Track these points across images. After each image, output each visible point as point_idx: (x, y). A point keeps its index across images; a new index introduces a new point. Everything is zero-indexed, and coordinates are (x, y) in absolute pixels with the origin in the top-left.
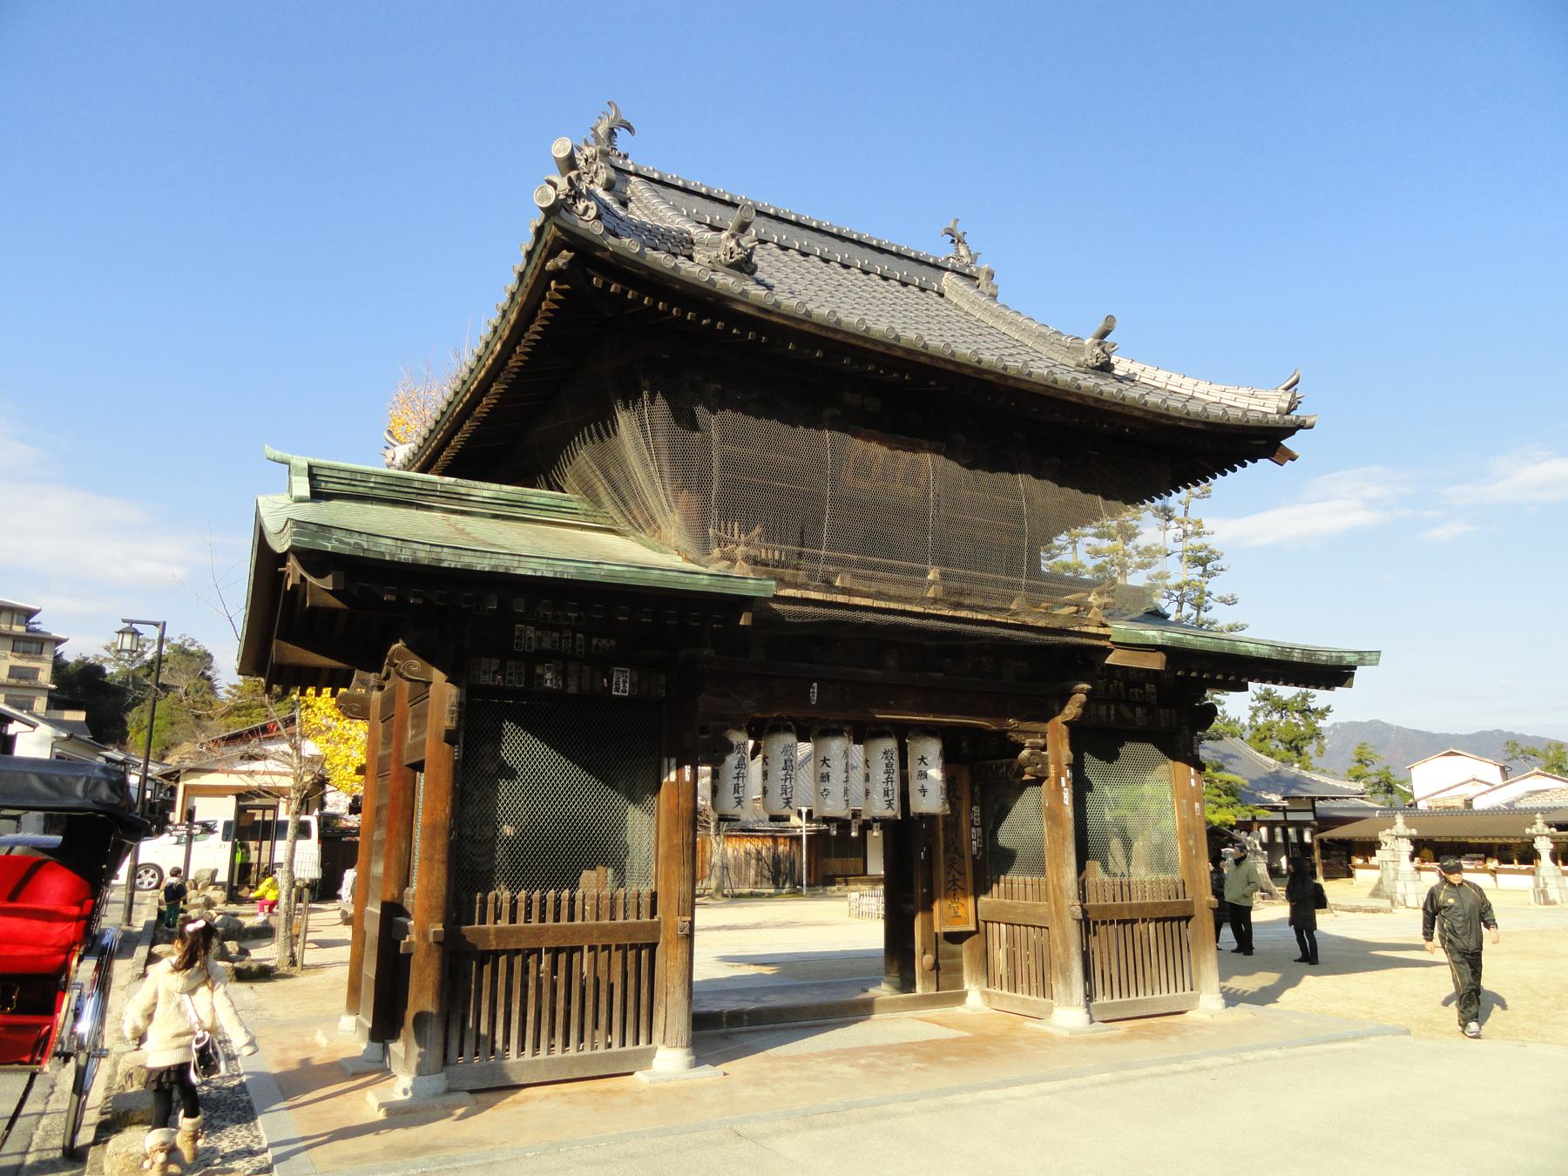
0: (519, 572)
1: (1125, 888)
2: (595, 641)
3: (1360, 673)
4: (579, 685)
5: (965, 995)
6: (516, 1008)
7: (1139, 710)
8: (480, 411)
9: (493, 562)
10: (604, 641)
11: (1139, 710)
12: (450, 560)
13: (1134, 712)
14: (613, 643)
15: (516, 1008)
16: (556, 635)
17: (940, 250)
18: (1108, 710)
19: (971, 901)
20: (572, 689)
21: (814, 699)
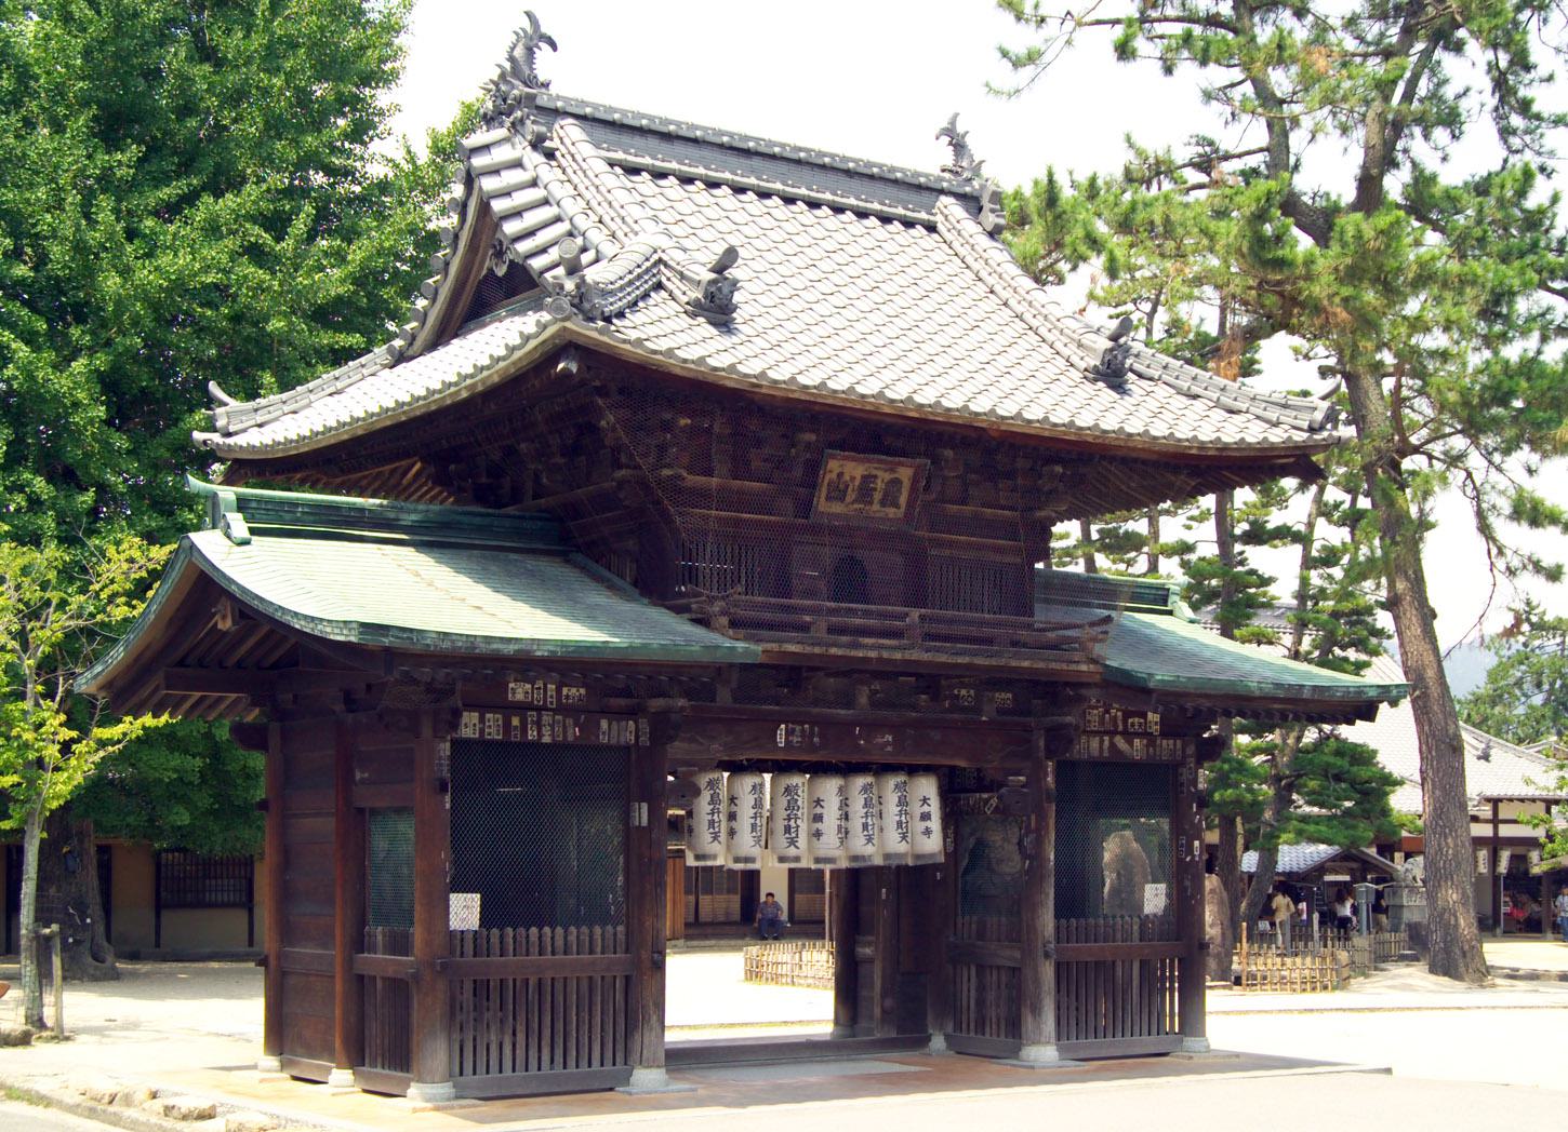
0: (539, 653)
1: (559, 986)
2: (565, 691)
4: (552, 735)
5: (928, 1039)
6: (560, 1026)
7: (1137, 742)
8: (541, 546)
9: (516, 647)
10: (574, 690)
11: (1137, 742)
12: (483, 648)
13: (1131, 744)
14: (582, 691)
15: (560, 1026)
16: (528, 686)
17: (931, 160)
18: (1102, 742)
19: (586, 272)
20: (547, 739)
21: (884, 897)
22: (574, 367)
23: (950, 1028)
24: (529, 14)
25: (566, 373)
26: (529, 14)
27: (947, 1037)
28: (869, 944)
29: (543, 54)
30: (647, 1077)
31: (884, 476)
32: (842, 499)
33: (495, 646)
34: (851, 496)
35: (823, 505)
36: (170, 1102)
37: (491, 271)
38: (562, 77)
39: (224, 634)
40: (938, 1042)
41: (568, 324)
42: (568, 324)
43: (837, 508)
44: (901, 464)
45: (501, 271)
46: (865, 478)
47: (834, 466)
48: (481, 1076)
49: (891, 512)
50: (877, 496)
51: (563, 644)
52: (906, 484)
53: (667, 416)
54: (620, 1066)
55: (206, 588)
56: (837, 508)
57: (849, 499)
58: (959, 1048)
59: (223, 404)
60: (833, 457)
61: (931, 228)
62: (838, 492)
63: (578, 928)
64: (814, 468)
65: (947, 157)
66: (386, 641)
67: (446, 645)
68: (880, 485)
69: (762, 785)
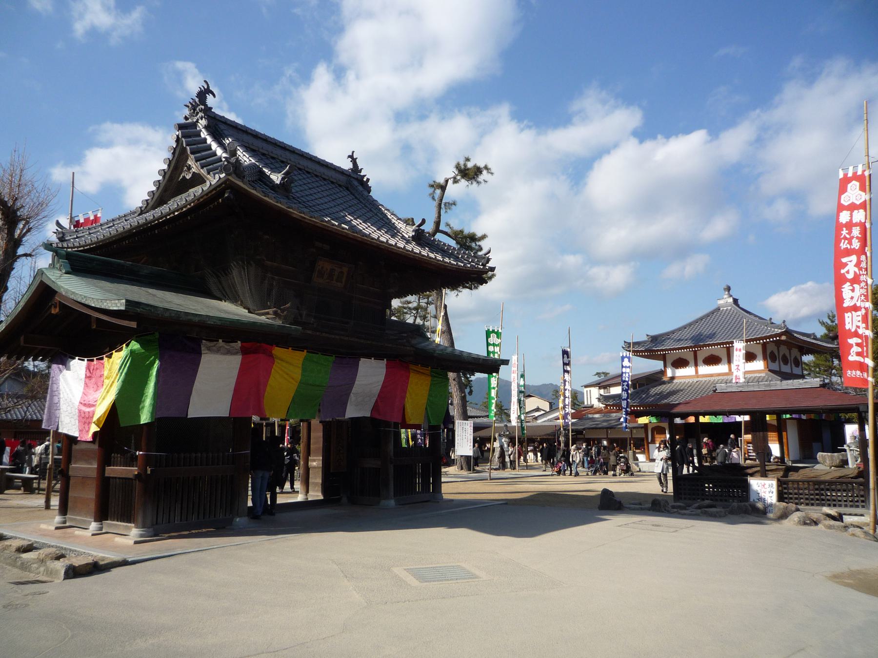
3: (502, 368)
28: (314, 461)
37: (184, 177)
39: (56, 315)
40: (344, 500)
42: (230, 178)
45: (188, 177)
67: (167, 315)
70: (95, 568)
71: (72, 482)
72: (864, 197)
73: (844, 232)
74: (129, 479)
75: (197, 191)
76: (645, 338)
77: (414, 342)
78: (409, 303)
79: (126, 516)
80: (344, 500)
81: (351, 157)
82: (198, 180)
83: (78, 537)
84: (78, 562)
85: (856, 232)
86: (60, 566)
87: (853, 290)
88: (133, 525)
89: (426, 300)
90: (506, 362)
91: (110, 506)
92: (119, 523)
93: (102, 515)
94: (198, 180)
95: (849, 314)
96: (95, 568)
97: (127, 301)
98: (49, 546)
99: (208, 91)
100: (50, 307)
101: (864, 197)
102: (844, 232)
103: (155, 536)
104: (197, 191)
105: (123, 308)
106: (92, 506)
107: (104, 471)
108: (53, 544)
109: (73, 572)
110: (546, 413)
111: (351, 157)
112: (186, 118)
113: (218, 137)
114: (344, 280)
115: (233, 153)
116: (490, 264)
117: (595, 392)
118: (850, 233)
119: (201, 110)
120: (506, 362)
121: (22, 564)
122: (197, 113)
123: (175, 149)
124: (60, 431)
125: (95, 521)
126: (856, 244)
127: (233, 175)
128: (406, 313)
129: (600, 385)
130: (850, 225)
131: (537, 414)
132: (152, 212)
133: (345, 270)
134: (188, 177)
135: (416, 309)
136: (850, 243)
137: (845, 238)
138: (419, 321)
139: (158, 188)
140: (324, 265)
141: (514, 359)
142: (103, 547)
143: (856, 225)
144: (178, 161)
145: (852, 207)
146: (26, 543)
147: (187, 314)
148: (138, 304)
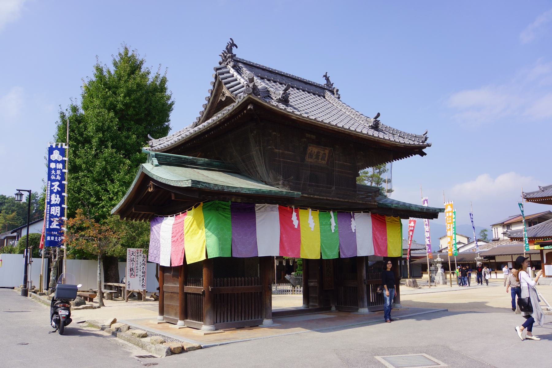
3: (440, 214)
5: (331, 307)
22: (252, 108)
23: (336, 305)
24: (231, 39)
25: (250, 108)
26: (231, 39)
27: (336, 307)
28: (312, 282)
29: (234, 48)
30: (267, 322)
31: (322, 152)
32: (311, 158)
33: (230, 189)
34: (314, 157)
35: (308, 160)
36: (134, 331)
37: (221, 100)
38: (238, 53)
39: (151, 192)
40: (333, 308)
41: (250, 96)
42: (250, 96)
43: (310, 160)
44: (326, 149)
45: (223, 99)
46: (318, 152)
47: (310, 148)
48: (222, 323)
49: (324, 162)
50: (320, 157)
51: (249, 189)
52: (327, 154)
53: (270, 131)
54: (259, 319)
55: (146, 178)
56: (310, 160)
57: (314, 158)
58: (339, 309)
59: (151, 140)
60: (310, 146)
61: (324, 97)
62: (311, 156)
63: (248, 277)
64: (305, 149)
65: (325, 82)
66: (199, 186)
67: (216, 188)
68: (321, 154)
69: (168, 305)
70: (182, 350)
71: (165, 294)
72: (60, 158)
73: (53, 172)
74: (199, 294)
75: (229, 109)
76: (538, 189)
77: (377, 199)
78: (367, 173)
79: (199, 317)
80: (333, 308)
81: (325, 76)
82: (229, 101)
83: (171, 329)
84: (174, 345)
85: (58, 172)
86: (164, 347)
87: (56, 197)
88: (202, 323)
89: (378, 171)
90: (442, 210)
91: (190, 310)
92: (194, 321)
93: (185, 315)
94: (229, 101)
95: (54, 207)
96: (182, 350)
97: (192, 181)
98: (156, 335)
99: (233, 45)
100: (148, 188)
101: (60, 158)
102: (53, 172)
103: (216, 330)
104: (229, 109)
105: (190, 185)
106: (178, 310)
107: (183, 288)
108: (157, 333)
109: (171, 352)
110: (465, 245)
111: (325, 76)
112: (220, 63)
113: (239, 71)
114: (326, 159)
115: (251, 80)
116: (428, 142)
117: (501, 230)
118: (56, 172)
119: (229, 57)
120: (442, 210)
121: (142, 345)
122: (227, 59)
123: (215, 83)
124: (188, 263)
125: (180, 320)
126: (58, 178)
127: (253, 94)
128: (365, 180)
129: (503, 225)
130: (56, 169)
131: (458, 246)
132: (204, 124)
133: (327, 152)
134: (223, 99)
135: (372, 177)
136: (56, 177)
137: (53, 174)
138: (374, 185)
139: (205, 109)
140: (313, 149)
141: (449, 209)
142: (186, 336)
143: (58, 169)
144: (217, 90)
145: (56, 162)
146: (143, 332)
147: (228, 187)
148: (199, 182)
